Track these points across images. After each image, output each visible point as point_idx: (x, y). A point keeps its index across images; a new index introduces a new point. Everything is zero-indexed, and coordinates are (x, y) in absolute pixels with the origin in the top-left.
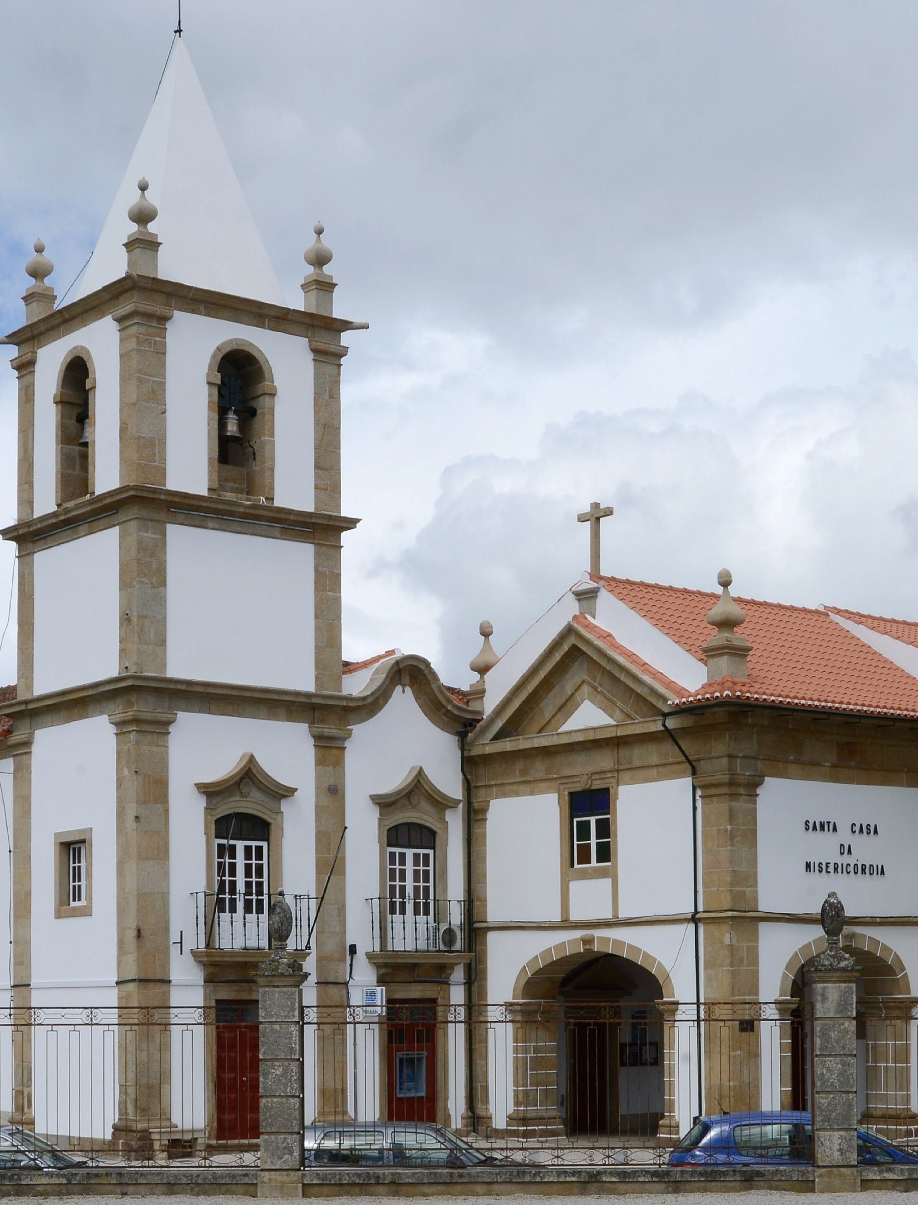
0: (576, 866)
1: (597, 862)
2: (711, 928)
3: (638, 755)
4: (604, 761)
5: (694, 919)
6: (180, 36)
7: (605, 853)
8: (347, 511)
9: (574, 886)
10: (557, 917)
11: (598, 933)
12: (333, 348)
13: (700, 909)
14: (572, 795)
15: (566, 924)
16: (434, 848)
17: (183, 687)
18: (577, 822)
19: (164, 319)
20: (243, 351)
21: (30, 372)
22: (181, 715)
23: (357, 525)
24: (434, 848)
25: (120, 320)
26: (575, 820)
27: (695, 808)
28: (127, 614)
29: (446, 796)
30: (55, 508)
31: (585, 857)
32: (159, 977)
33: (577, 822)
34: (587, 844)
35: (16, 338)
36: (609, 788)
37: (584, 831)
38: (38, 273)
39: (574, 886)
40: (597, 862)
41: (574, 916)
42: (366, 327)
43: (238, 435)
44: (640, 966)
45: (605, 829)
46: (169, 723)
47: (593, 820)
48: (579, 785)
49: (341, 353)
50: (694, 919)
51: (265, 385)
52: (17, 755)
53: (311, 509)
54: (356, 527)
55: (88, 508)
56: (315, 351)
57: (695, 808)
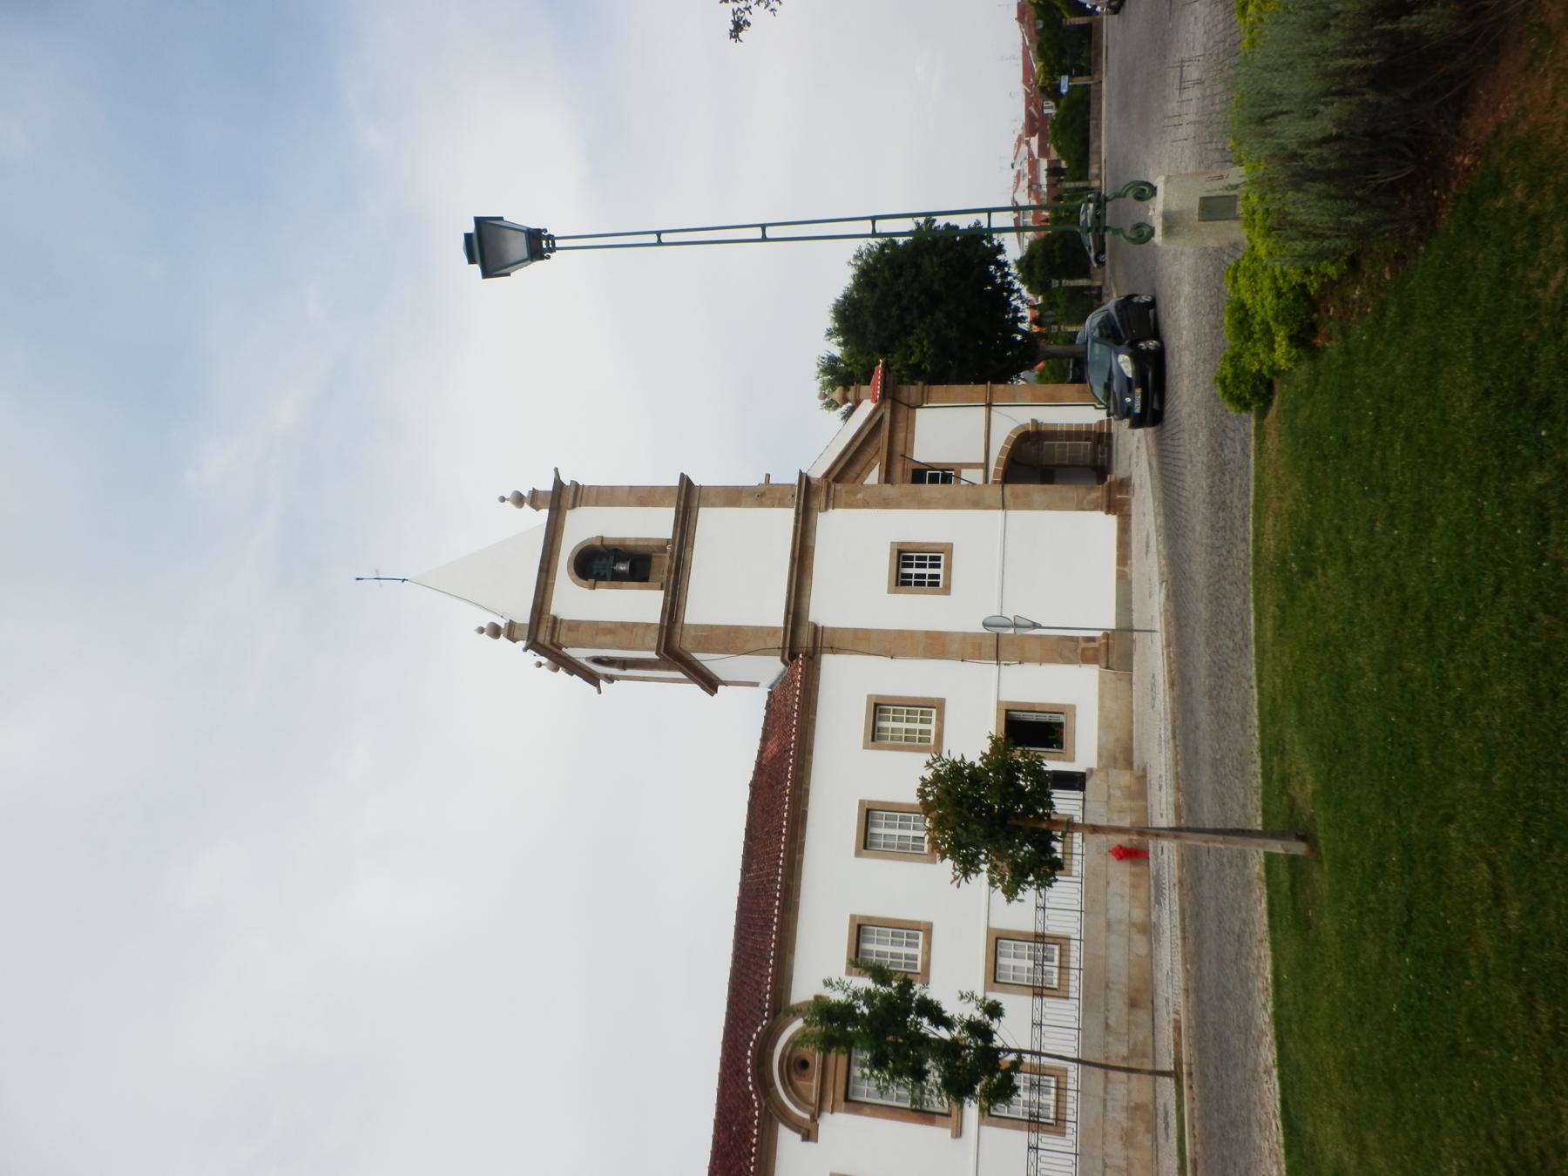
2: (995, 396)
3: (899, 448)
5: (989, 406)
6: (751, 13)
8: (675, 482)
10: (993, 214)
12: (573, 489)
17: (790, 616)
19: (555, 619)
20: (576, 557)
22: (811, 619)
27: (933, 407)
29: (1183, 911)
42: (556, 470)
43: (629, 563)
46: (816, 627)
49: (576, 486)
50: (989, 406)
51: (598, 543)
53: (673, 510)
55: (672, 576)
56: (574, 506)
57: (933, 407)
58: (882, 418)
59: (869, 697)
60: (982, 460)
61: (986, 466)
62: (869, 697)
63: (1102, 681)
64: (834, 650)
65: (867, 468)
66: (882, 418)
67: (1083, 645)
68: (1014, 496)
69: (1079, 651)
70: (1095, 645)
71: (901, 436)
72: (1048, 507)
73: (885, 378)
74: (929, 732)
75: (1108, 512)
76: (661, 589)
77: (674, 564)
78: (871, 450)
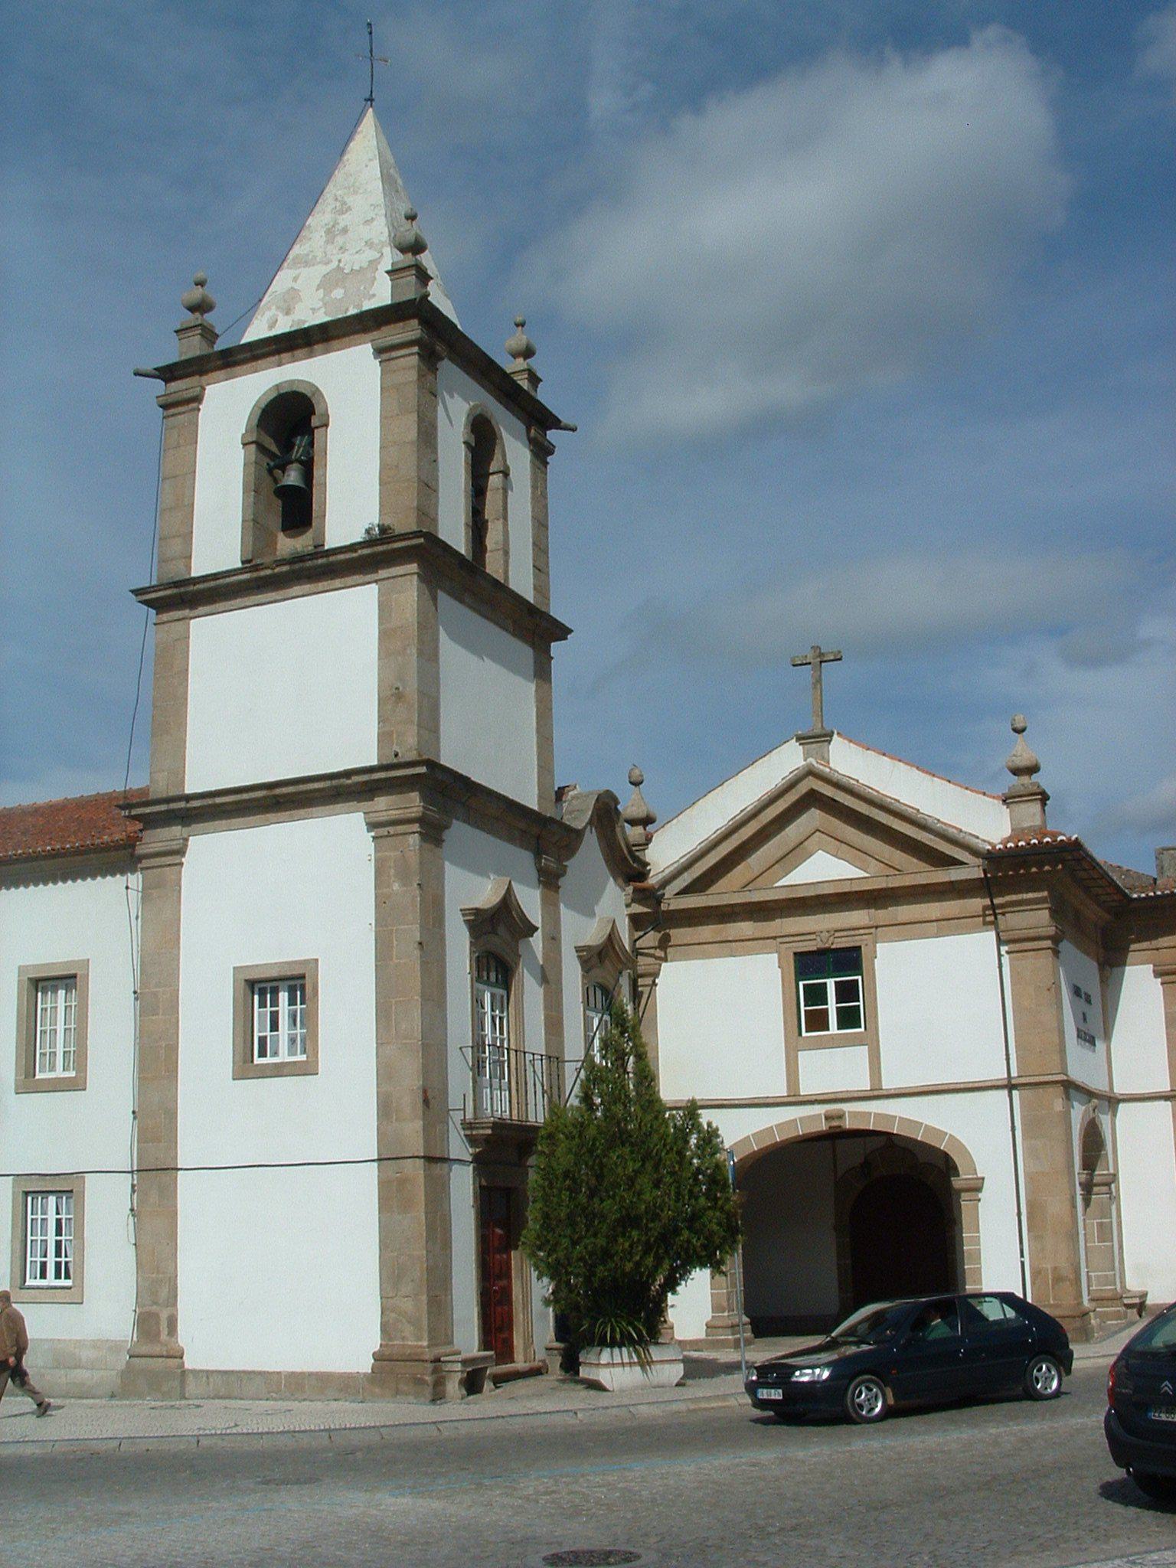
0: (804, 1034)
1: (838, 1029)
4: (858, 917)
7: (849, 1018)
9: (804, 1057)
10: (780, 1090)
11: (846, 1107)
13: (1014, 1074)
14: (799, 956)
15: (794, 1100)
16: (862, 975)
18: (857, 980)
21: (193, 410)
23: (569, 636)
24: (862, 975)
25: (379, 352)
26: (801, 984)
28: (397, 688)
30: (239, 565)
31: (817, 1021)
32: (172, 1166)
33: (804, 985)
34: (841, 1003)
35: (168, 373)
36: (860, 947)
37: (816, 995)
38: (201, 307)
39: (804, 1057)
40: (838, 1029)
41: (806, 1089)
42: (574, 430)
44: (920, 1142)
45: (847, 992)
46: (181, 852)
47: (831, 984)
48: (814, 943)
52: (147, 868)
54: (566, 639)
58: (955, 862)
59: (22, 970)
60: (888, 1083)
61: (876, 1094)
62: (22, 970)
63: (115, 1347)
64: (147, 895)
65: (842, 848)
66: (955, 862)
67: (164, 1315)
68: (402, 1182)
69: (154, 1308)
70: (164, 1336)
71: (933, 909)
72: (385, 1244)
73: (1003, 857)
74: (52, 1068)
75: (377, 1357)
76: (243, 562)
77: (268, 572)
78: (898, 857)
